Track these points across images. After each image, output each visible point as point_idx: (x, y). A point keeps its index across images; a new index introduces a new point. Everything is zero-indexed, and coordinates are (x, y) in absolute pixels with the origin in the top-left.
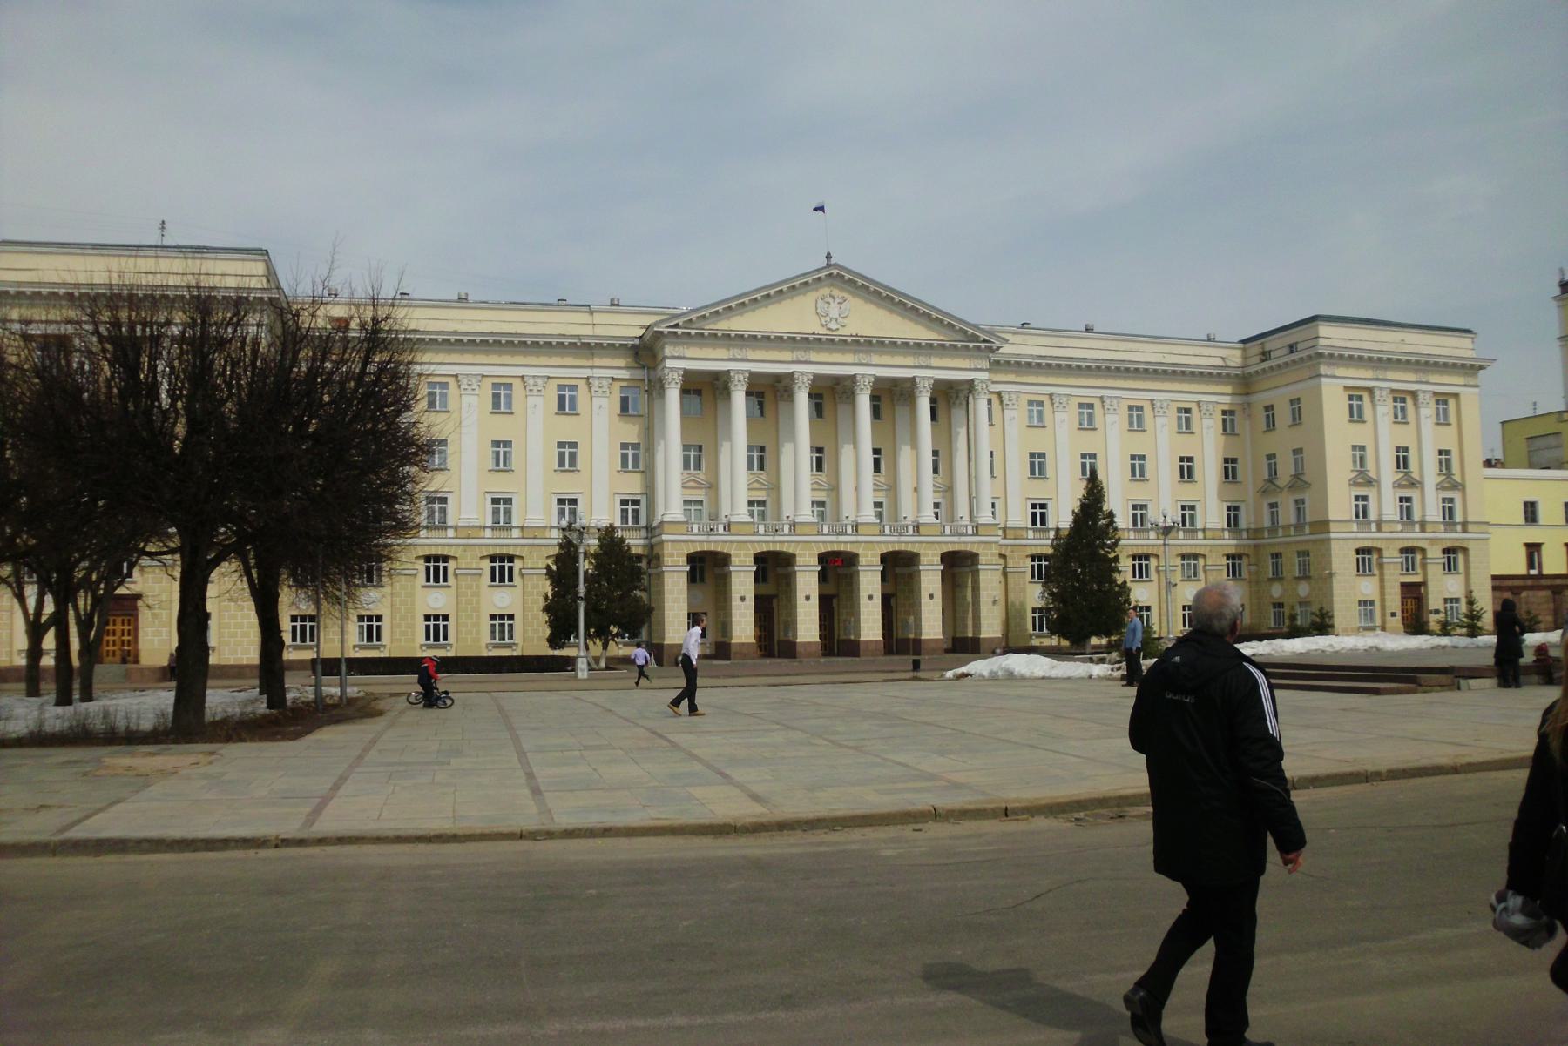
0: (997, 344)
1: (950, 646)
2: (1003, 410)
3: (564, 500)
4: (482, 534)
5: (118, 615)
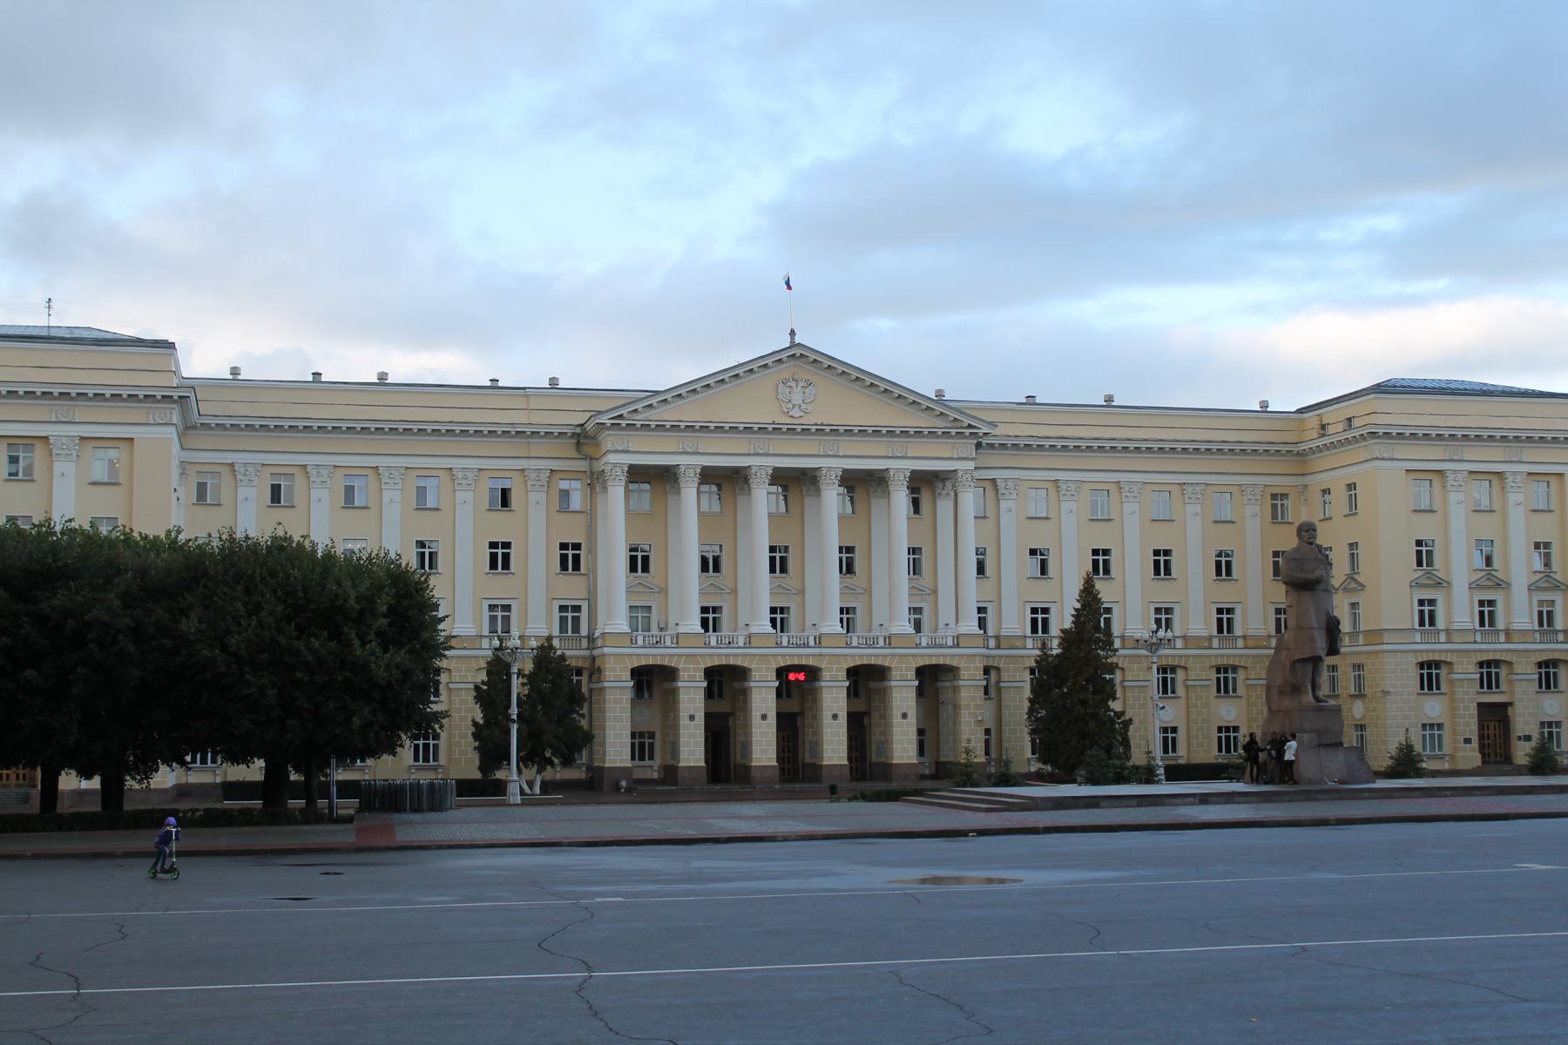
0: (985, 430)
1: (933, 772)
2: (998, 500)
3: (496, 606)
4: (1526, 639)
5: (1491, 721)
